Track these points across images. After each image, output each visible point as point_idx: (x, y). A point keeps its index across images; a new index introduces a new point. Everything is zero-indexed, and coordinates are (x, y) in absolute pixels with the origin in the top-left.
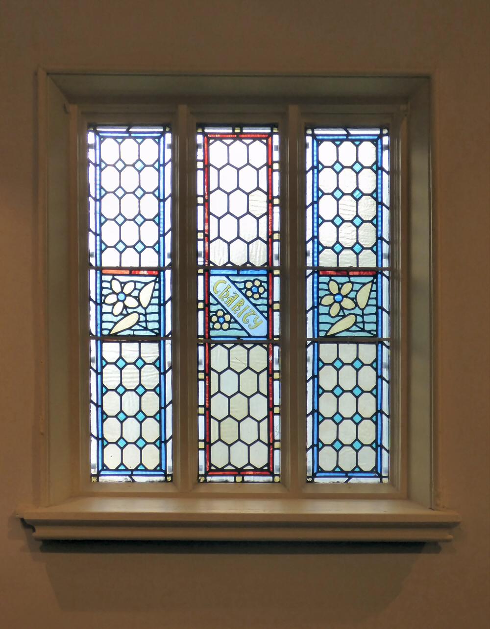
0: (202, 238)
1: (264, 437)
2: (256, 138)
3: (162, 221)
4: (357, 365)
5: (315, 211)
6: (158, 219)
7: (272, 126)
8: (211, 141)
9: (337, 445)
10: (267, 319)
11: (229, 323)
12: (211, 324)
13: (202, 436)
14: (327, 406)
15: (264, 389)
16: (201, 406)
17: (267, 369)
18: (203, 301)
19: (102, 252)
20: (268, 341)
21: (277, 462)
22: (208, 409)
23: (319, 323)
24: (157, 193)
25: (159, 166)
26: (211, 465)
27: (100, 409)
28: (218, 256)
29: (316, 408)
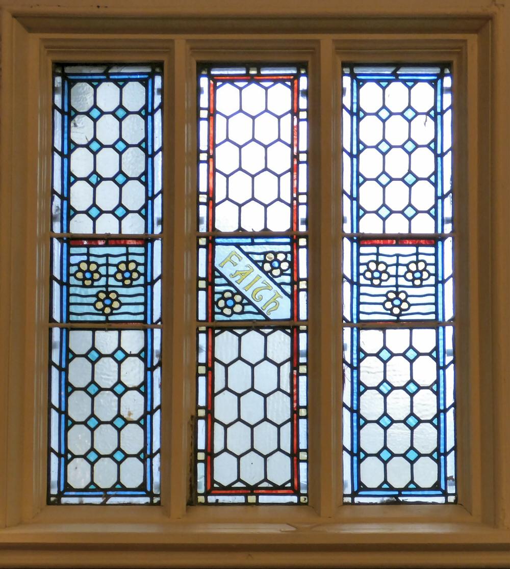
1: (286, 446)
2: (276, 80)
4: (411, 355)
5: (149, 403)
7: (299, 65)
8: (219, 84)
9: (385, 455)
10: (214, 269)
11: (264, 261)
12: (289, 258)
14: (134, 162)
15: (286, 385)
20: (291, 326)
21: (303, 479)
23: (359, 303)
26: (213, 482)
28: (226, 220)
29: (150, 159)
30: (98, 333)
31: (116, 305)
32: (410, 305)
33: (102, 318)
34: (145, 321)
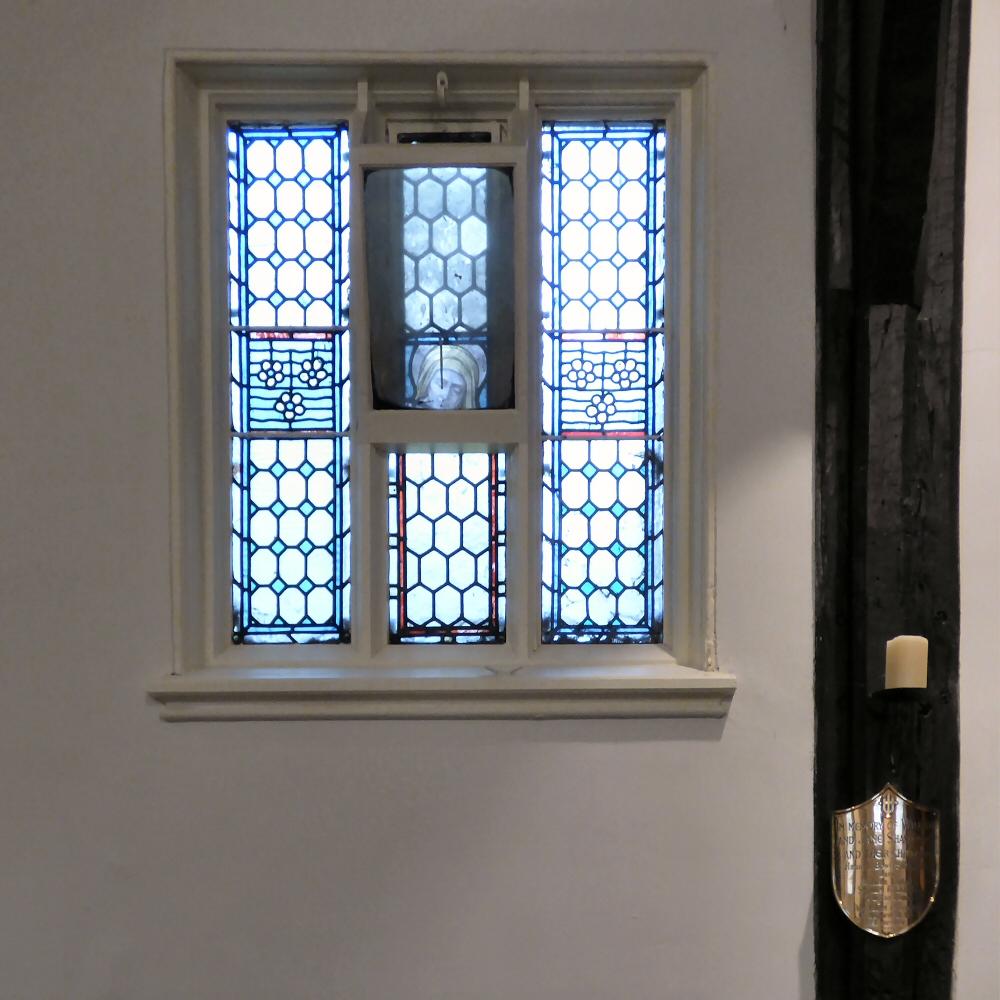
0: (395, 493)
3: (338, 549)
6: (331, 259)
13: (393, 580)
15: (484, 509)
16: (393, 535)
17: (489, 478)
18: (397, 586)
19: (248, 306)
22: (402, 539)
23: (249, 409)
24: (330, 220)
25: (334, 179)
26: (407, 620)
27: (245, 492)
30: (281, 442)
31: (299, 410)
32: (305, 409)
33: (286, 425)
34: (645, 430)
